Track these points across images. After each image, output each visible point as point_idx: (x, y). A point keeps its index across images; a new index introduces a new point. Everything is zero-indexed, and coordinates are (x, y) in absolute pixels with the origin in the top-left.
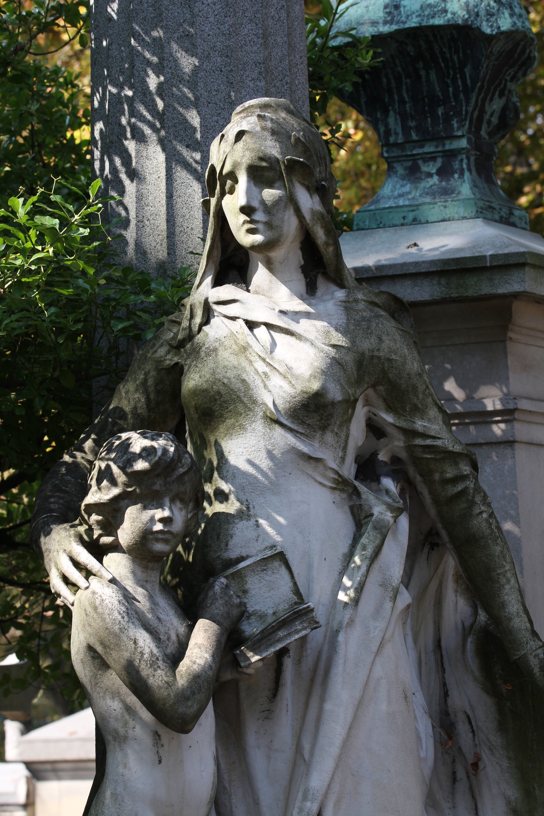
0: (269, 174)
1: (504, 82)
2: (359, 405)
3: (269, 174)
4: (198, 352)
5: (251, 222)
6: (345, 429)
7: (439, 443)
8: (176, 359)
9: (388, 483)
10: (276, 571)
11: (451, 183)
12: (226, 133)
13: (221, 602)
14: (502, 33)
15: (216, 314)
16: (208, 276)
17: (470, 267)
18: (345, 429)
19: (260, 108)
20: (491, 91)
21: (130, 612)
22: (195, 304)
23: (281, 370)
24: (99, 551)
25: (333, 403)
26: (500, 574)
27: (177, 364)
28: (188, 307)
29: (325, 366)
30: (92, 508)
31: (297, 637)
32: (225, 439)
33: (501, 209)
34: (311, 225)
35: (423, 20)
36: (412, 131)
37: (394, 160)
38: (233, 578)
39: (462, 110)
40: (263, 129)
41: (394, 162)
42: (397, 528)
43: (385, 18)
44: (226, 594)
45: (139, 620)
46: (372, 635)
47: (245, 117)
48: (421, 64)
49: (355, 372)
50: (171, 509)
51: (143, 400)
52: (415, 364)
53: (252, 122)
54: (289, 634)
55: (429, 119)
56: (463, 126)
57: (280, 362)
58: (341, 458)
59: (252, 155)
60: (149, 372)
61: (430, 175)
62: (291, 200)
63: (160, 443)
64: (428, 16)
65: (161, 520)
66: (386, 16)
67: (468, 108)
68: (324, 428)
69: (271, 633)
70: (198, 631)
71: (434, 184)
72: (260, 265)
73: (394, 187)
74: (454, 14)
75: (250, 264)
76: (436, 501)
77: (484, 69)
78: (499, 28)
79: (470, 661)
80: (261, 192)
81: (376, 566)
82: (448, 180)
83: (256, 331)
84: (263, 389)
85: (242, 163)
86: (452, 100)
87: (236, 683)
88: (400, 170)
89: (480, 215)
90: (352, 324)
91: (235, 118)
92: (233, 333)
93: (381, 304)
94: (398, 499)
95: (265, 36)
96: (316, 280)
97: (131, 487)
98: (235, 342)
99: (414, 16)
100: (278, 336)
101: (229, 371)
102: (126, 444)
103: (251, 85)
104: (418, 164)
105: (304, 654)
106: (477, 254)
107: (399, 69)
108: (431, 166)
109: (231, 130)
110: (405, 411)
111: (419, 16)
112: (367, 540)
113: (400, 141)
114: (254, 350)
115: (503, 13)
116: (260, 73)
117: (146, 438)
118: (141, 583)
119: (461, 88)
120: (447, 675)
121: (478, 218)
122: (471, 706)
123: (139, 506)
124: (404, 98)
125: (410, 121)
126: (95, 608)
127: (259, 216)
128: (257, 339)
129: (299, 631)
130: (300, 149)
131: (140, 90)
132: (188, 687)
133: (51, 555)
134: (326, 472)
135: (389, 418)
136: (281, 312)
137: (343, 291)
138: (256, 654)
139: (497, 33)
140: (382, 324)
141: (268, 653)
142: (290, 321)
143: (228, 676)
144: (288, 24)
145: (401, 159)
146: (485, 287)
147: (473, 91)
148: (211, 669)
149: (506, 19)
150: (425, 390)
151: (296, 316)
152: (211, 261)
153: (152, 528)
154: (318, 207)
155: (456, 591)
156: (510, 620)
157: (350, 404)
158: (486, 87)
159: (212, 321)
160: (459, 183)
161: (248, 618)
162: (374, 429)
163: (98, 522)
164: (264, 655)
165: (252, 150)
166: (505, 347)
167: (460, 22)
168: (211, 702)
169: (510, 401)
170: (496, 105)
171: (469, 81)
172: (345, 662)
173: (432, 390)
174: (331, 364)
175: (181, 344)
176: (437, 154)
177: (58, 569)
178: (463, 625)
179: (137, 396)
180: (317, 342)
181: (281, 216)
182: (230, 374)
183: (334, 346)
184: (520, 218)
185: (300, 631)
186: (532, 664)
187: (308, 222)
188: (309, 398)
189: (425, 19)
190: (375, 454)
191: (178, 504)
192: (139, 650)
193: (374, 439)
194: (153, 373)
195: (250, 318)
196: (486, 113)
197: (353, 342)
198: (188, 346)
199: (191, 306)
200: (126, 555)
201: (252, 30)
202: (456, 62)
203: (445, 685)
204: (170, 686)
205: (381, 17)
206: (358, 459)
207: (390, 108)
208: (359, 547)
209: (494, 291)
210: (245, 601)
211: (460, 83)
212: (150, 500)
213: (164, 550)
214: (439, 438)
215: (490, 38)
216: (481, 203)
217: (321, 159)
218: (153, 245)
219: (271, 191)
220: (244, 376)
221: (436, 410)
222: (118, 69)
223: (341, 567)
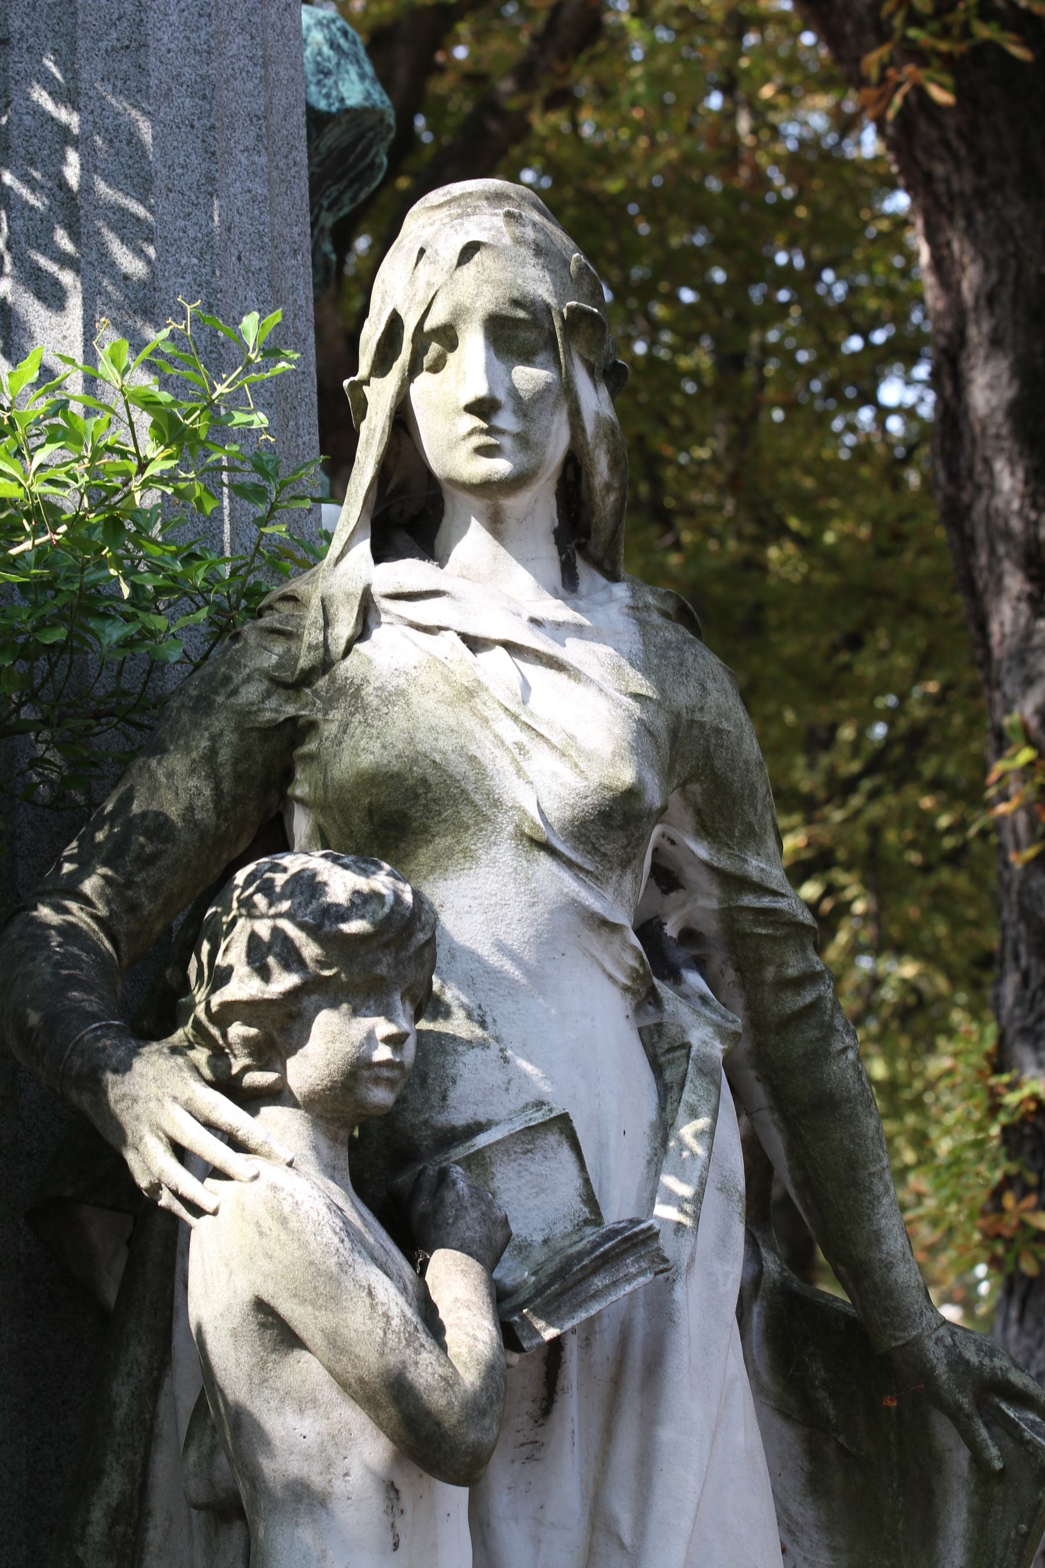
0: (527, 335)
3: (527, 335)
5: (490, 431)
8: (290, 710)
10: (550, 1154)
13: (474, 1214)
14: (349, 111)
15: (384, 618)
16: (360, 541)
19: (487, 198)
22: (331, 597)
23: (555, 740)
28: (315, 602)
31: (628, 1288)
32: (431, 878)
34: (591, 447)
40: (519, 241)
44: (481, 1198)
46: (722, 1290)
51: (208, 793)
54: (615, 1284)
59: (498, 293)
60: (221, 734)
62: (568, 390)
65: (388, 1040)
69: (580, 1281)
72: (474, 522)
75: (445, 521)
78: (342, 100)
80: (509, 372)
84: (515, 777)
92: (435, 658)
97: (330, 968)
100: (535, 672)
105: (597, 1328)
110: (731, 836)
115: (347, 72)
116: (259, 138)
126: (284, 1221)
127: (506, 420)
131: (23, 153)
132: (482, 1390)
135: (702, 851)
136: (534, 621)
138: (551, 1324)
139: (338, 110)
140: (703, 657)
149: (352, 83)
151: (559, 629)
153: (370, 1056)
156: (889, 1266)
159: (376, 633)
163: (246, 1041)
175: (307, 678)
179: (192, 783)
181: (545, 423)
182: (445, 744)
183: (636, 696)
185: (634, 1277)
186: (932, 1356)
187: (589, 439)
188: (614, 799)
192: (380, 1309)
193: (657, 891)
194: (230, 737)
195: (472, 631)
198: (322, 683)
199: (323, 600)
200: (301, 1112)
201: (244, 47)
204: (451, 1386)
219: (528, 370)
220: (473, 750)
223: (648, 1150)
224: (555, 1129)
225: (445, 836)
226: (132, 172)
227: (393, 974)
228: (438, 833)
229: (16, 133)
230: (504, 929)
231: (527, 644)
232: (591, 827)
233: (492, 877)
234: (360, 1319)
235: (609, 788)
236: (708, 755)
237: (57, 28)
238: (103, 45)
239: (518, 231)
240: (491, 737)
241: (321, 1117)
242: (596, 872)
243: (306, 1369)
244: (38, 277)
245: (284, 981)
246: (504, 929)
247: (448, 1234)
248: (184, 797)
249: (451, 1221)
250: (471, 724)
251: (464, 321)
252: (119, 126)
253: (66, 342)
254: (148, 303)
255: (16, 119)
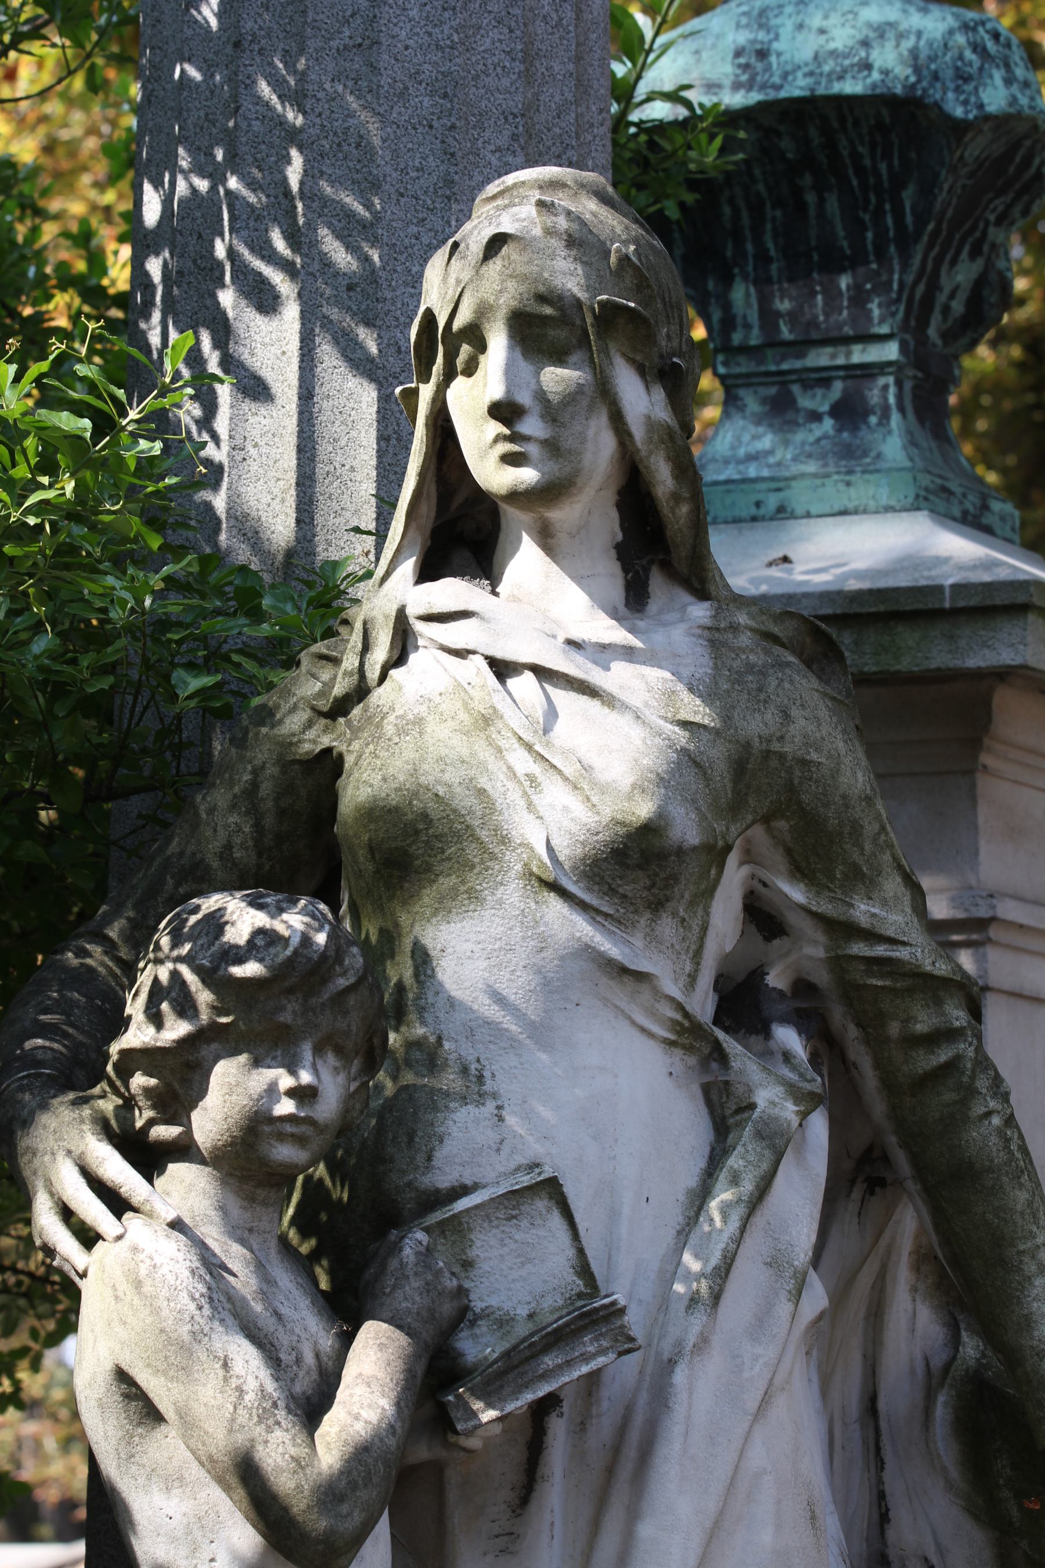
0: (558, 334)
1: (981, 225)
2: (732, 860)
3: (558, 334)
4: (379, 726)
5: (513, 438)
6: (700, 912)
7: (902, 953)
8: (326, 741)
9: (788, 1037)
11: (861, 434)
12: (464, 238)
14: (988, 118)
15: (421, 642)
16: (406, 559)
17: (908, 608)
18: (700, 912)
19: (541, 187)
20: (955, 243)
21: (215, 1296)
22: (373, 619)
23: (568, 771)
24: (149, 1159)
25: (680, 852)
26: (1024, 1252)
27: (328, 751)
28: (358, 626)
29: (665, 767)
30: (131, 1061)
31: (585, 1369)
32: (434, 920)
33: (964, 495)
34: (643, 453)
35: (819, 83)
36: (781, 322)
37: (740, 382)
38: (443, 1232)
39: (890, 282)
40: (549, 232)
41: (737, 386)
42: (804, 1139)
43: (737, 76)
44: (428, 1267)
45: (236, 1315)
46: (746, 1375)
47: (506, 207)
48: (807, 180)
49: (729, 786)
50: (316, 1072)
51: (247, 830)
52: (860, 775)
53: (523, 216)
54: (569, 1364)
55: (819, 297)
56: (893, 314)
57: (565, 753)
58: (689, 975)
59: (522, 288)
60: (263, 767)
61: (815, 417)
62: (604, 392)
63: (293, 922)
64: (829, 74)
65: (291, 1093)
66: (738, 71)
67: (905, 277)
68: (657, 906)
69: (527, 1360)
70: (365, 1347)
71: (826, 436)
72: (526, 538)
73: (738, 439)
74: (886, 72)
75: (502, 536)
76: (889, 1084)
77: (944, 194)
78: (981, 106)
79: (940, 1445)
81: (759, 1220)
82: (855, 429)
83: (511, 683)
84: (525, 812)
85: (499, 306)
86: (872, 258)
87: (437, 1469)
88: (752, 403)
89: (923, 504)
90: (725, 680)
91: (482, 210)
92: (459, 684)
93: (785, 640)
94: (811, 1073)
95: (528, 58)
96: (648, 579)
97: (227, 1015)
98: (465, 705)
99: (800, 74)
100: (562, 698)
101: (449, 768)
102: (216, 923)
103: (494, 161)
104: (790, 393)
105: (594, 1412)
106: (923, 582)
107: (761, 187)
108: (819, 397)
109: (476, 233)
110: (832, 878)
111: (811, 74)
112: (741, 1162)
113: (753, 342)
114: (507, 725)
115: (991, 77)
116: (515, 137)
117: (260, 907)
118: (239, 1232)
119: (891, 234)
120: (887, 1476)
121: (918, 509)
122: (938, 1545)
123: (243, 1058)
124: (768, 250)
125: (777, 301)
126: (138, 1285)
127: (532, 426)
128: (514, 701)
129: (593, 1357)
130: (629, 281)
133: (37, 1162)
134: (657, 1005)
136: (570, 643)
137: (707, 604)
138: (490, 1405)
139: (976, 118)
140: (791, 682)
141: (519, 1403)
142: (590, 665)
143: (422, 1452)
144: (577, 36)
145: (755, 380)
146: (938, 654)
147: (917, 239)
148: (394, 1434)
150: (879, 833)
152: (413, 525)
153: (271, 1110)
154: (663, 413)
155: (914, 1290)
157: (715, 854)
158: (944, 233)
159: (413, 658)
160: (878, 436)
161: (473, 1324)
162: (762, 917)
163: (147, 1091)
164: (510, 1407)
165: (523, 278)
166: (973, 787)
167: (899, 90)
168: (386, 1512)
169: (980, 902)
170: (963, 274)
171: (909, 219)
172: (687, 1433)
173: (892, 835)
174: (678, 764)
175: (341, 708)
176: (833, 374)
177: (52, 1194)
178: (928, 1365)
180: (647, 713)
181: (579, 428)
182: (452, 776)
183: (685, 724)
184: (1003, 518)
185: (593, 1356)
187: (639, 445)
188: (629, 836)
189: (824, 81)
190: (758, 974)
191: (331, 1058)
192: (234, 1382)
194: (271, 770)
195: (499, 654)
196: (941, 290)
197: (726, 718)
198: (356, 711)
199: (365, 623)
200: (208, 1169)
201: (500, 41)
202: (885, 177)
203: (881, 1496)
205: (726, 75)
206: (720, 983)
207: (736, 271)
208: (723, 1176)
209: (958, 663)
210: (467, 1284)
211: (889, 221)
212: (268, 1044)
213: (296, 1160)
214: (904, 944)
215: (960, 128)
216: (925, 480)
217: (672, 307)
218: (264, 501)
219: (559, 371)
220: (483, 782)
221: (899, 880)
222: (202, 114)
223: (681, 1219)
224: (544, 1194)
225: (449, 875)
226: (359, 176)
227: (300, 1022)
228: (442, 872)
229: (244, 140)
230: (508, 976)
231: (555, 668)
232: (604, 866)
233: (497, 920)
234: (211, 1393)
235: (623, 824)
236: (791, 788)
237: (288, 28)
238: (334, 44)
239: (550, 220)
240: (504, 769)
241: (231, 1175)
242: (617, 915)
243: (167, 1446)
244: (261, 291)
245: (176, 1030)
246: (508, 976)
247: (382, 1305)
248: (222, 834)
249: (388, 1290)
250: (486, 754)
251: (488, 320)
252: (348, 128)
253: (284, 358)
254: (371, 315)
255: (244, 125)
